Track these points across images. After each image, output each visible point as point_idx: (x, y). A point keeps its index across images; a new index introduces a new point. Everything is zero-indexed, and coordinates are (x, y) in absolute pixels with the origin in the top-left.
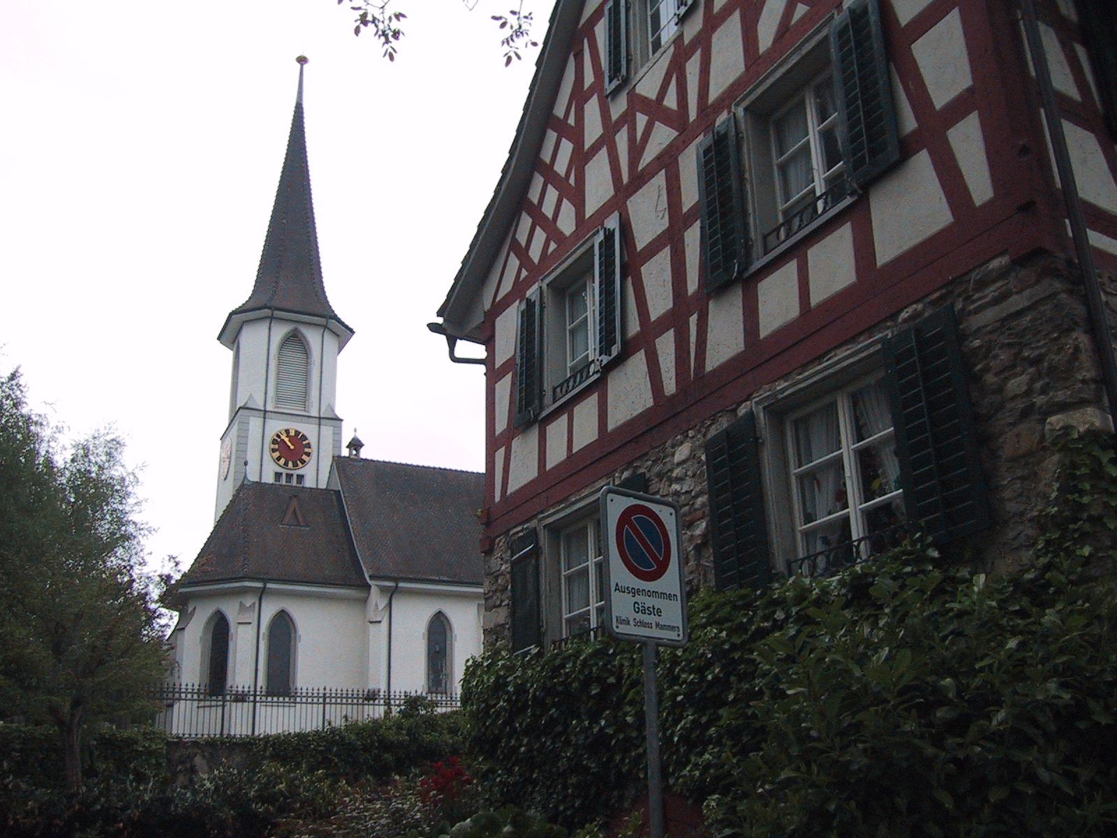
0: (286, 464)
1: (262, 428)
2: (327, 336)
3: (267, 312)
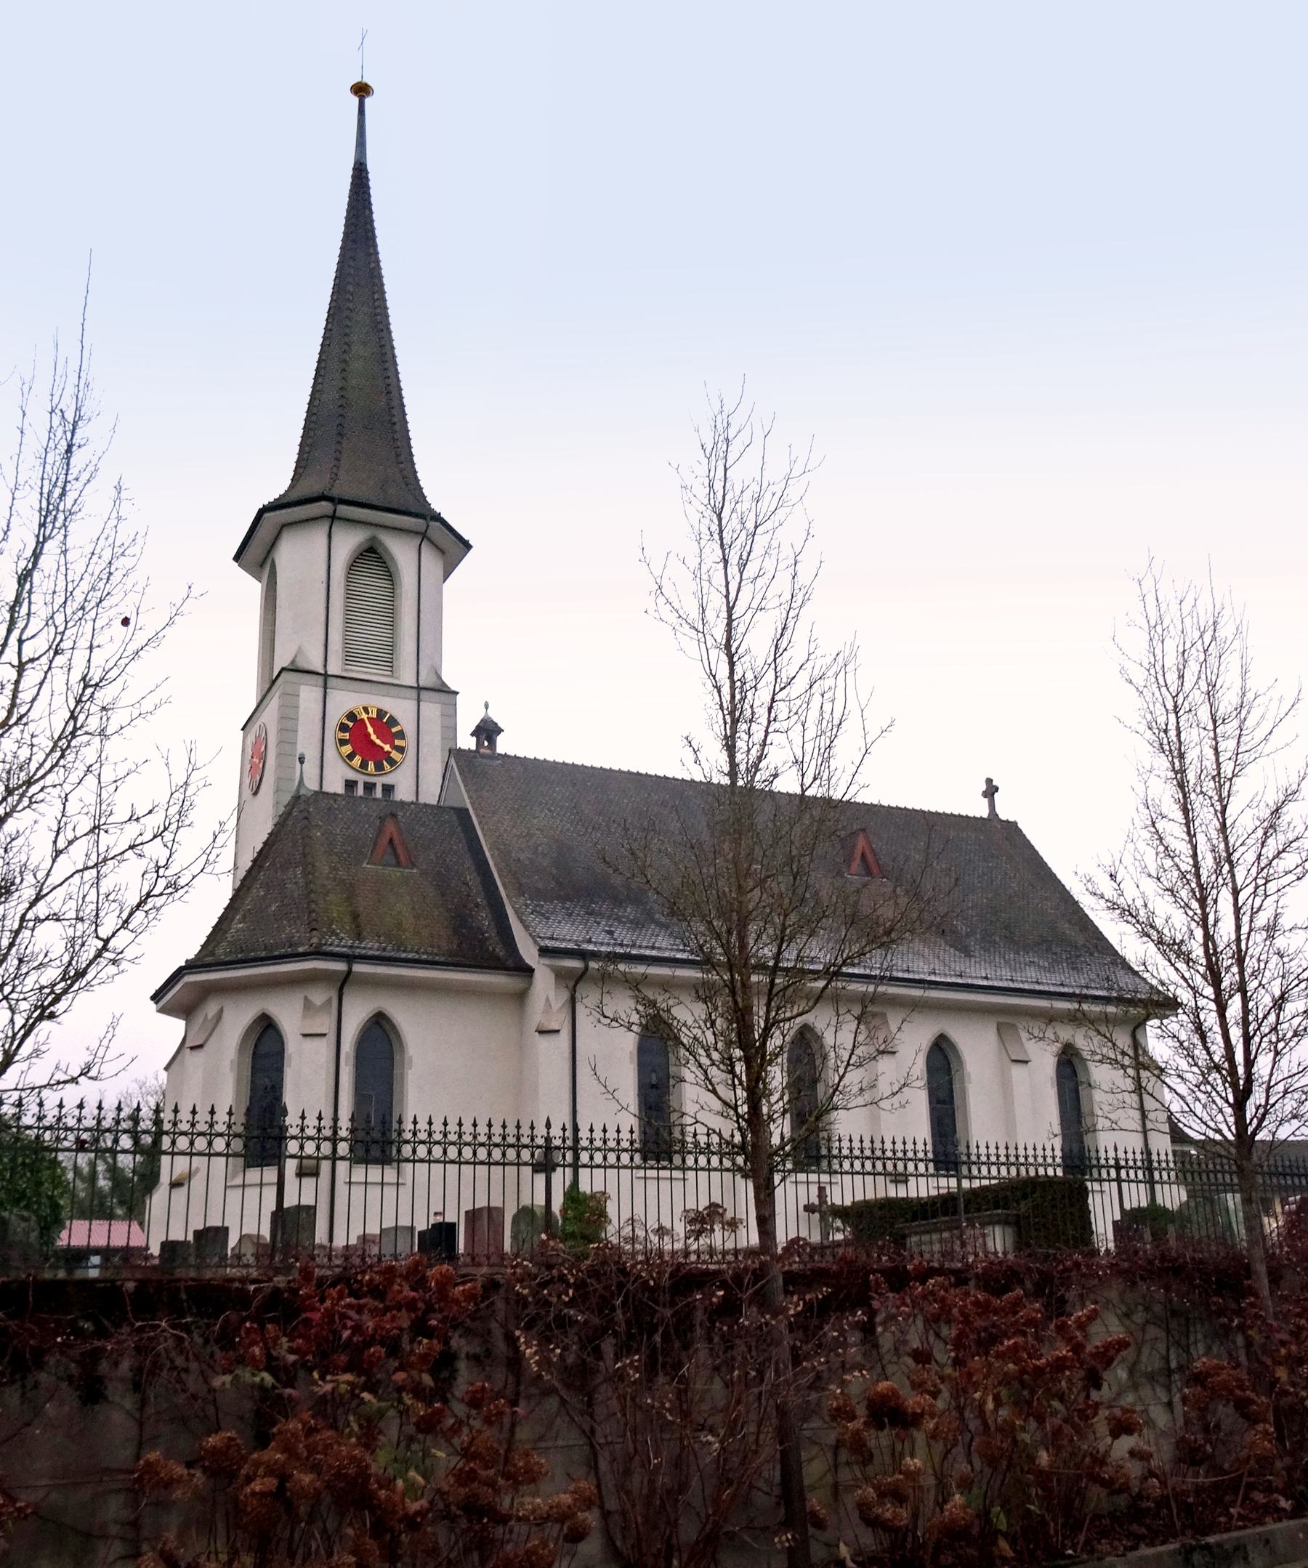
0: (364, 765)
1: (321, 704)
2: (427, 553)
3: (325, 507)
